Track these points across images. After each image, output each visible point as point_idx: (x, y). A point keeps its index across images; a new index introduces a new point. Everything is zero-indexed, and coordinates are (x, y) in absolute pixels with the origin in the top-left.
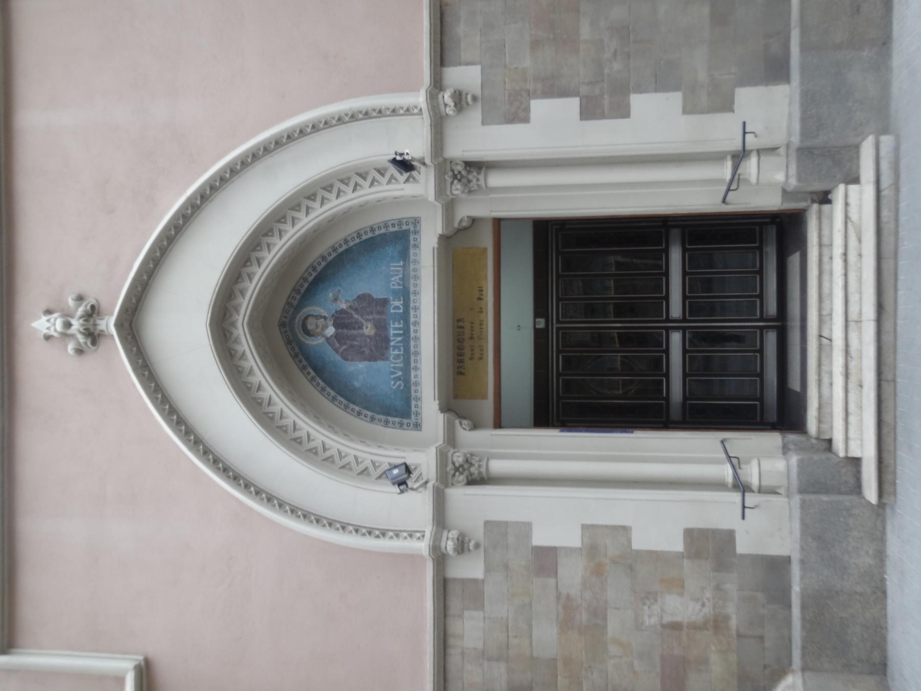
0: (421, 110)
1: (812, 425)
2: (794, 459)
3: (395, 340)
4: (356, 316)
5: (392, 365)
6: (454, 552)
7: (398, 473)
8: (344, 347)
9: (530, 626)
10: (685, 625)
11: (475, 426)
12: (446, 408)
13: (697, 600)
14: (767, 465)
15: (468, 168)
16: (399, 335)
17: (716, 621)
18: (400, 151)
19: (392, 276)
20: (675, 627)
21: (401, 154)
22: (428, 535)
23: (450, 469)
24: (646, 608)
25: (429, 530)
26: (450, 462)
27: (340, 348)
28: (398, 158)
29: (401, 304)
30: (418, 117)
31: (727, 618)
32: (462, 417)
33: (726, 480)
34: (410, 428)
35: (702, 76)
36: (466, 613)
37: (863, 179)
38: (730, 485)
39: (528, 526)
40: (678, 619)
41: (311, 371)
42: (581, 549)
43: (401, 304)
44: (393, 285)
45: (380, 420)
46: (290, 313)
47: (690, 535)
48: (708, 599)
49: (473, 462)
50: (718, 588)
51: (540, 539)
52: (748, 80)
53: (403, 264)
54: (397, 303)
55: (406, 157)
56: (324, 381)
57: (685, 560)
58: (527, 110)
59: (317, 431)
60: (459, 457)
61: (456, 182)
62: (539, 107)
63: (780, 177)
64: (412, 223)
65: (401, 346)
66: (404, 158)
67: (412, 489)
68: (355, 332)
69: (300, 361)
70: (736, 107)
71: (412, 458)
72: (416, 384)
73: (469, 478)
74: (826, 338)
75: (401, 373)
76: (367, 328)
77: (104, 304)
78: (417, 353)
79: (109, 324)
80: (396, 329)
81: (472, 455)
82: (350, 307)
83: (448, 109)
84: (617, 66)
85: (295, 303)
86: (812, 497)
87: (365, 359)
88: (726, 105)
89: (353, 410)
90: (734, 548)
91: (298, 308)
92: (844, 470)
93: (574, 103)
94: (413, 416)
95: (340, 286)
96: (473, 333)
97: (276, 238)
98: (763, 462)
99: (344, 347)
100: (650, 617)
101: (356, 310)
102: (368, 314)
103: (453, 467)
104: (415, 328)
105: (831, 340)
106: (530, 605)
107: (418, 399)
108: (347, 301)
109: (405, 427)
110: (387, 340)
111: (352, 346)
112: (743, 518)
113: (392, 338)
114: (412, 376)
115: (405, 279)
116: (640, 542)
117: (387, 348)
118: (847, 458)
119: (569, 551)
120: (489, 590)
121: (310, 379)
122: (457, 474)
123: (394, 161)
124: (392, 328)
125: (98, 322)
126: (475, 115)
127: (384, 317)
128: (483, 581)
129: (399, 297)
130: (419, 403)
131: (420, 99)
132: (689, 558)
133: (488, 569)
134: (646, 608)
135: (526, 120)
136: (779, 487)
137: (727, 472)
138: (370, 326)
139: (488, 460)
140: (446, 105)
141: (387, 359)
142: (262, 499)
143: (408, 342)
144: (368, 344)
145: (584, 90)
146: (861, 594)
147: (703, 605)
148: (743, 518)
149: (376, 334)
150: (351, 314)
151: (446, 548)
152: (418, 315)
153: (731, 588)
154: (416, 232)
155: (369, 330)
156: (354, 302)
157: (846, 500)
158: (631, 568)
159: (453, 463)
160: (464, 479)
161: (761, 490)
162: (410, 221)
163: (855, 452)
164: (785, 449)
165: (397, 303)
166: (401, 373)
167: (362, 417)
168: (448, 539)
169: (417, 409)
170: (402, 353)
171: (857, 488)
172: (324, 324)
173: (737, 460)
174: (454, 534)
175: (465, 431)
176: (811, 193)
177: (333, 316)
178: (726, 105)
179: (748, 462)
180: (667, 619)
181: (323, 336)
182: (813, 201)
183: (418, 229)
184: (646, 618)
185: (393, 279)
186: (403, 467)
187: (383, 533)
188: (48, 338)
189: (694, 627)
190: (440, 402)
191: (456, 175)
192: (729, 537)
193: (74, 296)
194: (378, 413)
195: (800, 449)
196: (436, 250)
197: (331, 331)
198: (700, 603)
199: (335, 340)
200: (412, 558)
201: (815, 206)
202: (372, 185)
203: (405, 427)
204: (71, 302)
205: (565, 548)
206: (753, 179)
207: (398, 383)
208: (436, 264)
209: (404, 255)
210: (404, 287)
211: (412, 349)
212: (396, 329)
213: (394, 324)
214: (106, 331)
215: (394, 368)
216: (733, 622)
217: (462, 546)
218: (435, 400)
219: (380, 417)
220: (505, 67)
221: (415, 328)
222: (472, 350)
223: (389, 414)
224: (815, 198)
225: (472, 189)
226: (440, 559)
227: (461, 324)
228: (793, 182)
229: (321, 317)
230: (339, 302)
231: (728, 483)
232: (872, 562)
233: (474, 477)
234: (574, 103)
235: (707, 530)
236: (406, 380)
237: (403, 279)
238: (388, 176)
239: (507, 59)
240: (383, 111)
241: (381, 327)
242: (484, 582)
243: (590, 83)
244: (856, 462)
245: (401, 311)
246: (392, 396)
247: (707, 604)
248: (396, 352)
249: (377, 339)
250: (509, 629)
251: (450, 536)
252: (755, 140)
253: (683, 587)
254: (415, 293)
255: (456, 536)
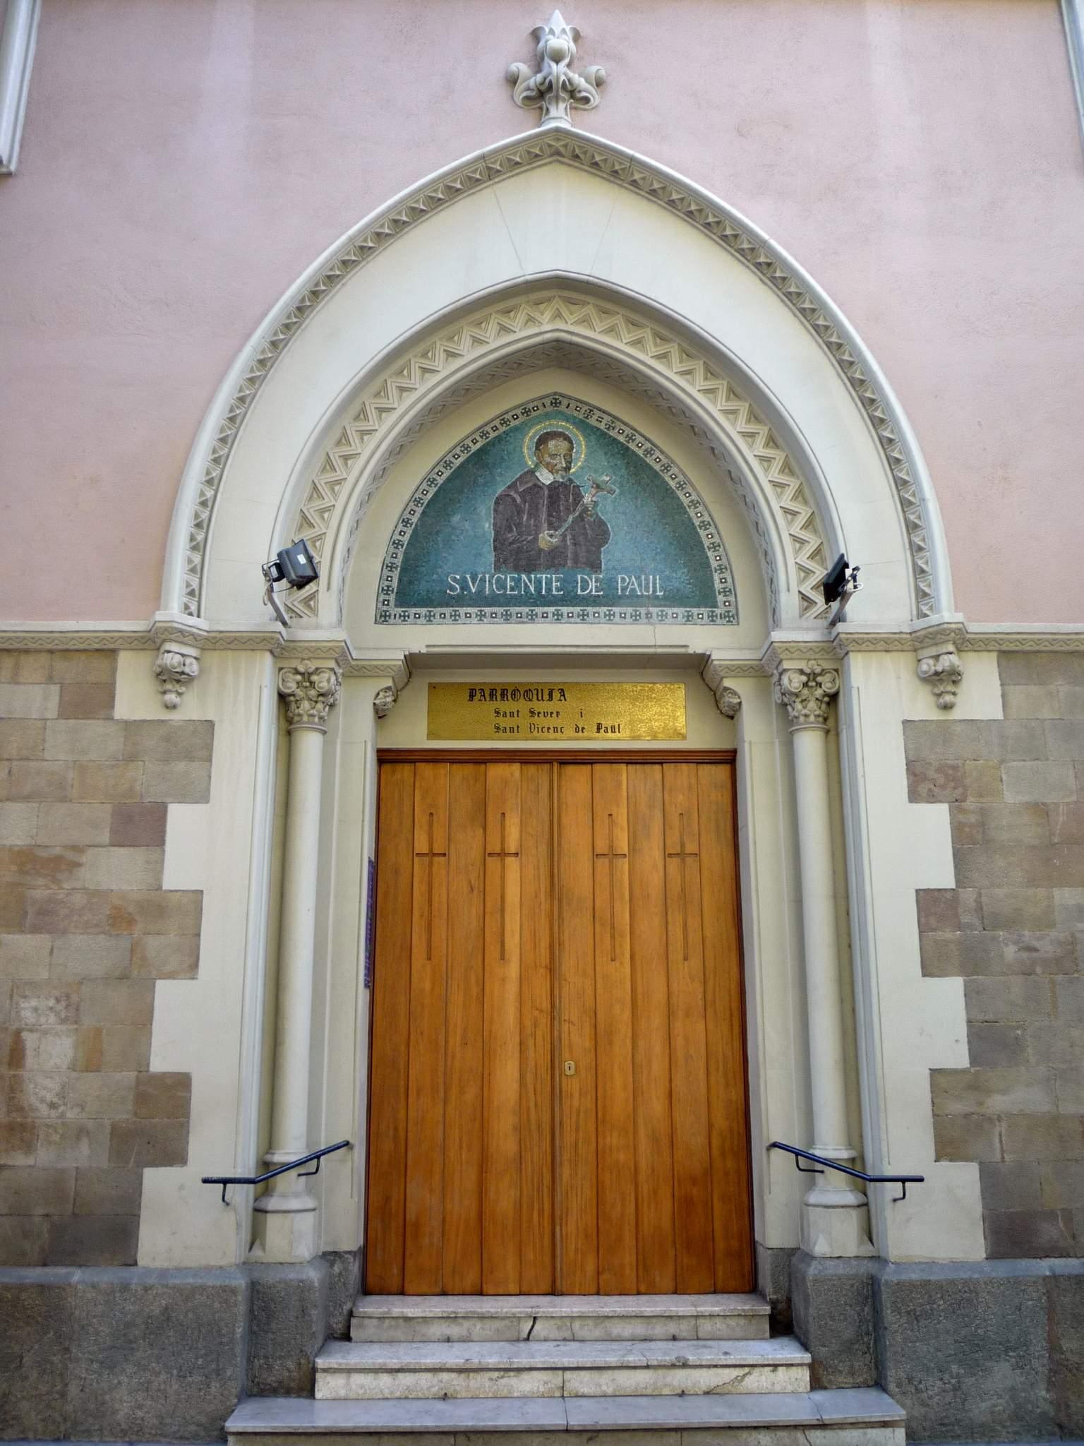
0: (926, 616)
1: (372, 1306)
2: (314, 1275)
3: (530, 582)
4: (571, 518)
5: (487, 576)
6: (160, 666)
7: (299, 562)
8: (519, 500)
9: (27, 798)
10: (19, 1072)
11: (380, 715)
12: (415, 664)
13: (63, 1096)
14: (306, 1223)
15: (826, 699)
16: (539, 589)
17: (23, 1127)
18: (859, 575)
19: (638, 578)
20: (16, 1056)
21: (854, 577)
22: (192, 621)
23: (306, 665)
24: (51, 1003)
25: (200, 624)
26: (318, 664)
27: (516, 492)
28: (848, 572)
29: (591, 591)
30: (915, 612)
31: (28, 1147)
32: (397, 693)
33: (277, 1152)
34: (380, 605)
35: (997, 1103)
36: (55, 689)
37: (819, 1396)
38: (268, 1158)
39: (203, 797)
40: (30, 1061)
41: (478, 446)
42: (160, 888)
43: (591, 591)
44: (623, 579)
45: (395, 556)
46: (576, 414)
47: (181, 1082)
48: (62, 1115)
49: (320, 706)
50: (82, 1132)
51: (179, 817)
52: (991, 1180)
53: (658, 596)
54: (592, 585)
55: (850, 586)
56: (462, 465)
57: (133, 1074)
58: (932, 798)
59: (378, 446)
60: (329, 681)
61: (804, 678)
62: (937, 816)
63: (821, 1247)
64: (728, 612)
65: (520, 591)
66: (849, 581)
67: (271, 590)
68: (544, 516)
69: (495, 429)
70: (944, 1164)
71: (327, 595)
72: (455, 617)
73: (292, 698)
74: (533, 1327)
75: (474, 591)
76: (551, 536)
77: (591, 118)
78: (507, 618)
79: (560, 117)
80: (549, 582)
81: (332, 706)
82: (585, 510)
83: (931, 662)
84: (1010, 952)
85: (592, 421)
86: (242, 1308)
87: (497, 533)
88: (947, 1148)
89: (412, 512)
90: (153, 1164)
91: (583, 425)
92: (291, 1364)
93: (944, 878)
94: (400, 610)
95: (622, 493)
96: (541, 715)
97: (702, 384)
98: (310, 1217)
99: (519, 500)
100: (36, 1009)
101: (580, 516)
102: (574, 537)
103: (311, 670)
104: (550, 615)
105: (528, 1339)
106: (64, 799)
107: (430, 618)
108: (595, 504)
109: (382, 597)
110: (530, 569)
111: (520, 512)
112: (206, 1181)
113: (533, 576)
114: (469, 610)
115: (633, 599)
116: (167, 993)
117: (516, 569)
118: (314, 1370)
119: (157, 867)
120: (94, 728)
121: (465, 442)
122: (299, 677)
123: (842, 565)
124: (551, 578)
125: (562, 106)
126: (923, 708)
127: (569, 563)
128: (111, 718)
129: (602, 590)
130: (422, 620)
131: (947, 613)
132: (138, 1082)
133: (131, 727)
134: (51, 1003)
135: (914, 796)
136: (263, 1247)
137: (291, 1149)
138: (554, 540)
139: (324, 733)
140: (937, 657)
141: (497, 569)
142: (263, 352)
143: (525, 605)
144: (524, 537)
145: (968, 895)
146: (63, 1395)
147: (53, 1106)
148: (206, 1181)
149: (540, 550)
150: (574, 510)
151: (169, 652)
152: (572, 620)
153: (83, 1156)
154: (712, 618)
155: (547, 539)
156: (595, 516)
157: (236, 1371)
158: (123, 977)
159: (317, 671)
160: (289, 688)
161: (259, 1212)
162: (732, 609)
163: (326, 1386)
164: (330, 1257)
165: (592, 585)
166: (474, 591)
167: (400, 527)
168: (183, 655)
169: (412, 616)
170: (508, 592)
171: (258, 1390)
172: (558, 466)
173: (314, 1170)
174: (192, 668)
175: (374, 695)
176: (789, 1300)
177: (571, 481)
178: (947, 1148)
179: (310, 1191)
180: (30, 1039)
181: (537, 466)
182: (774, 1304)
183: (719, 621)
184: (34, 1003)
185: (633, 579)
186: (309, 573)
187: (197, 546)
188: (536, 35)
189: (14, 1089)
190: (423, 654)
191: (814, 680)
192: (174, 1155)
193: (603, 73)
194: (405, 553)
195: (331, 1286)
196: (682, 650)
197: (546, 478)
198: (55, 1100)
199: (530, 485)
200: (157, 597)
201: (767, 1309)
202: (795, 539)
203: (382, 597)
204: (593, 69)
205: (161, 862)
206: (813, 1198)
207: (457, 586)
208: (660, 650)
209: (673, 598)
210: (620, 597)
211: (514, 610)
212: (549, 582)
213: (557, 581)
214: (547, 117)
215: (483, 580)
216: (19, 1159)
217: (170, 678)
218: (428, 646)
219: (400, 556)
220: (1002, 761)
221: (550, 615)
222: (512, 714)
223: (404, 570)
224: (780, 1306)
225: (789, 708)
226: (152, 641)
227: (556, 695)
228: (812, 1270)
229: (569, 463)
230: (594, 491)
231: (273, 1154)
232: (120, 1416)
233: (293, 706)
234: (944, 878)
235: (187, 1114)
236: (459, 601)
237: (633, 593)
238: (811, 565)
239: (1015, 763)
240: (922, 554)
241: (554, 559)
242: (108, 719)
243: (979, 908)
244: (307, 1389)
245: (579, 592)
246: (435, 577)
247: (53, 1113)
248: (509, 583)
249: (533, 552)
250: (25, 763)
251: (188, 661)
252: (889, 1198)
253: (87, 1069)
254: (610, 615)
255: (187, 670)
